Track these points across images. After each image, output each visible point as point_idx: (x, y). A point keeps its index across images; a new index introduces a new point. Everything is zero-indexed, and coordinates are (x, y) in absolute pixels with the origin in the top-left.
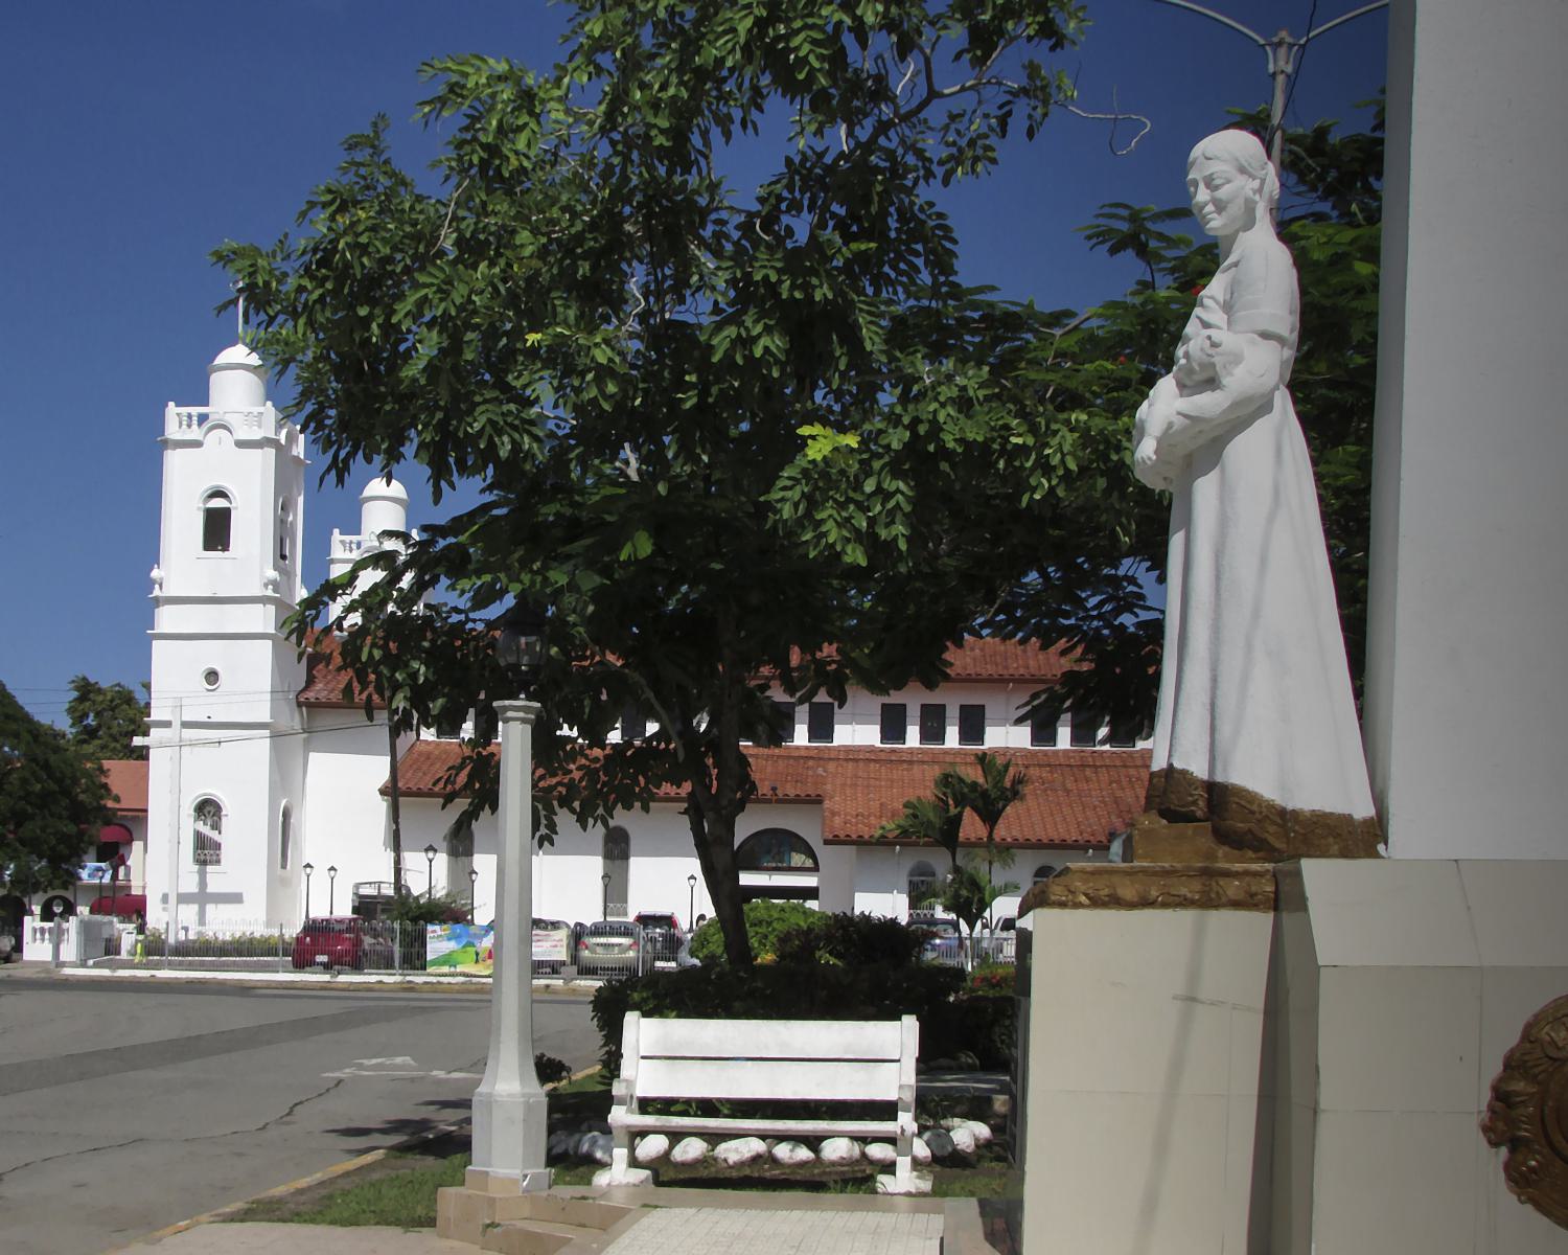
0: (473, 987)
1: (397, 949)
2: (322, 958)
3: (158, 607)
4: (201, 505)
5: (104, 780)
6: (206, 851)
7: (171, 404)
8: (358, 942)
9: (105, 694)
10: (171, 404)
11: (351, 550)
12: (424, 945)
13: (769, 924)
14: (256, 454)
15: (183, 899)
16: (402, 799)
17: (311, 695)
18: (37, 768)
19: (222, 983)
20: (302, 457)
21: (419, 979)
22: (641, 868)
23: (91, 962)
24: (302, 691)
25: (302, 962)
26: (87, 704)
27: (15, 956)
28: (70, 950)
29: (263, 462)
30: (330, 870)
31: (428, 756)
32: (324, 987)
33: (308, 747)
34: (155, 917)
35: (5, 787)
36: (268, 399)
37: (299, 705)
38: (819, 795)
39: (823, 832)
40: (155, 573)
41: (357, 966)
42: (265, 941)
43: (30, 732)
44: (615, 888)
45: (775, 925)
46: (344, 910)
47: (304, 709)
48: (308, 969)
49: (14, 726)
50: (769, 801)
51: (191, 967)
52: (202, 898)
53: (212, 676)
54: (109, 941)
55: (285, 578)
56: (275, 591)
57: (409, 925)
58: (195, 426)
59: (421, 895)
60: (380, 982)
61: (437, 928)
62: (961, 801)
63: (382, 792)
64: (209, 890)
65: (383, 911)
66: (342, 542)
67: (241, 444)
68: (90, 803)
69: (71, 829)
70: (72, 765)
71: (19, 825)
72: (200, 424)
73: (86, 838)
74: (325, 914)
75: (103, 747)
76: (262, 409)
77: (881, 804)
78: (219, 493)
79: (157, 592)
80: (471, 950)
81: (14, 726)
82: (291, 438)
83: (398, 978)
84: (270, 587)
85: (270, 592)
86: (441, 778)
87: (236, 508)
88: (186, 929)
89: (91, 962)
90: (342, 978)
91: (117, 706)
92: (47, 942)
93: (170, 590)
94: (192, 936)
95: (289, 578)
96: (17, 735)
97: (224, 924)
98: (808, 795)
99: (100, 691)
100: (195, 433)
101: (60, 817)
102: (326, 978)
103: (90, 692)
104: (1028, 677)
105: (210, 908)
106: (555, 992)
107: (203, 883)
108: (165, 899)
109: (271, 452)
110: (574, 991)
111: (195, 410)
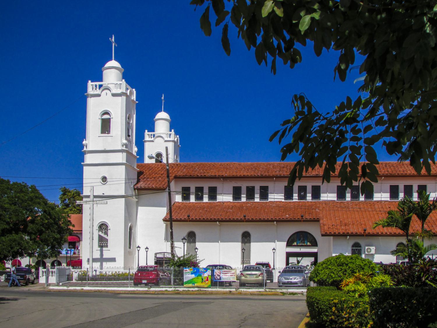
0: (203, 292)
1: (172, 277)
2: (144, 281)
3: (85, 154)
4: (100, 117)
5: (69, 219)
6: (103, 243)
7: (90, 81)
8: (158, 275)
9: (71, 193)
10: (90, 81)
11: (151, 137)
12: (182, 276)
13: (347, 265)
14: (119, 98)
15: (95, 260)
16: (173, 223)
17: (139, 185)
18: (46, 215)
19: (107, 292)
20: (135, 100)
21: (181, 289)
22: (255, 247)
23: (61, 284)
24: (136, 184)
25: (137, 282)
26: (66, 196)
27: (35, 282)
28: (53, 279)
29: (121, 101)
30: (146, 249)
31: (179, 207)
32: (146, 293)
33: (138, 204)
34: (85, 266)
35: (35, 221)
36: (123, 78)
37: (135, 189)
38: (318, 219)
39: (321, 231)
40: (84, 142)
41: (157, 284)
42: (123, 274)
43: (44, 202)
44: (245, 254)
45: (349, 265)
46: (151, 263)
47: (136, 191)
48: (139, 286)
49: (38, 200)
50: (300, 221)
51: (97, 285)
52: (102, 260)
53: (104, 179)
54: (68, 275)
55: (129, 143)
56: (126, 147)
57: (177, 268)
58: (98, 89)
59: (182, 257)
60: (166, 290)
61: (188, 269)
62: (410, 211)
63: (165, 220)
64: (104, 257)
65: (166, 263)
66: (148, 135)
67: (114, 95)
68: (65, 227)
69: (58, 236)
70: (58, 214)
71: (40, 235)
72: (99, 89)
73: (63, 239)
74: (145, 265)
75: (71, 210)
76: (121, 82)
77: (341, 221)
78: (106, 113)
79: (85, 149)
80: (200, 278)
81: (38, 200)
82: (131, 93)
83: (173, 289)
84: (124, 146)
85: (124, 148)
86: (278, 132)
87: (112, 118)
88: (96, 271)
89: (61, 284)
90: (152, 289)
91: (75, 197)
92: (44, 276)
93: (90, 148)
94: (98, 273)
95: (131, 143)
96: (39, 203)
97: (109, 268)
98: (314, 219)
99: (69, 192)
100: (98, 92)
101: (54, 232)
102: (146, 289)
103: (66, 192)
104: (389, 175)
105: (104, 264)
106: (233, 294)
107: (102, 254)
108: (88, 260)
109: (124, 98)
110: (241, 293)
111: (98, 83)
